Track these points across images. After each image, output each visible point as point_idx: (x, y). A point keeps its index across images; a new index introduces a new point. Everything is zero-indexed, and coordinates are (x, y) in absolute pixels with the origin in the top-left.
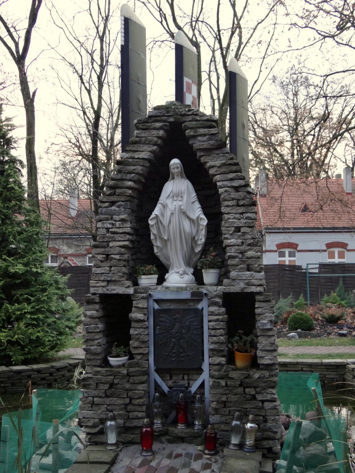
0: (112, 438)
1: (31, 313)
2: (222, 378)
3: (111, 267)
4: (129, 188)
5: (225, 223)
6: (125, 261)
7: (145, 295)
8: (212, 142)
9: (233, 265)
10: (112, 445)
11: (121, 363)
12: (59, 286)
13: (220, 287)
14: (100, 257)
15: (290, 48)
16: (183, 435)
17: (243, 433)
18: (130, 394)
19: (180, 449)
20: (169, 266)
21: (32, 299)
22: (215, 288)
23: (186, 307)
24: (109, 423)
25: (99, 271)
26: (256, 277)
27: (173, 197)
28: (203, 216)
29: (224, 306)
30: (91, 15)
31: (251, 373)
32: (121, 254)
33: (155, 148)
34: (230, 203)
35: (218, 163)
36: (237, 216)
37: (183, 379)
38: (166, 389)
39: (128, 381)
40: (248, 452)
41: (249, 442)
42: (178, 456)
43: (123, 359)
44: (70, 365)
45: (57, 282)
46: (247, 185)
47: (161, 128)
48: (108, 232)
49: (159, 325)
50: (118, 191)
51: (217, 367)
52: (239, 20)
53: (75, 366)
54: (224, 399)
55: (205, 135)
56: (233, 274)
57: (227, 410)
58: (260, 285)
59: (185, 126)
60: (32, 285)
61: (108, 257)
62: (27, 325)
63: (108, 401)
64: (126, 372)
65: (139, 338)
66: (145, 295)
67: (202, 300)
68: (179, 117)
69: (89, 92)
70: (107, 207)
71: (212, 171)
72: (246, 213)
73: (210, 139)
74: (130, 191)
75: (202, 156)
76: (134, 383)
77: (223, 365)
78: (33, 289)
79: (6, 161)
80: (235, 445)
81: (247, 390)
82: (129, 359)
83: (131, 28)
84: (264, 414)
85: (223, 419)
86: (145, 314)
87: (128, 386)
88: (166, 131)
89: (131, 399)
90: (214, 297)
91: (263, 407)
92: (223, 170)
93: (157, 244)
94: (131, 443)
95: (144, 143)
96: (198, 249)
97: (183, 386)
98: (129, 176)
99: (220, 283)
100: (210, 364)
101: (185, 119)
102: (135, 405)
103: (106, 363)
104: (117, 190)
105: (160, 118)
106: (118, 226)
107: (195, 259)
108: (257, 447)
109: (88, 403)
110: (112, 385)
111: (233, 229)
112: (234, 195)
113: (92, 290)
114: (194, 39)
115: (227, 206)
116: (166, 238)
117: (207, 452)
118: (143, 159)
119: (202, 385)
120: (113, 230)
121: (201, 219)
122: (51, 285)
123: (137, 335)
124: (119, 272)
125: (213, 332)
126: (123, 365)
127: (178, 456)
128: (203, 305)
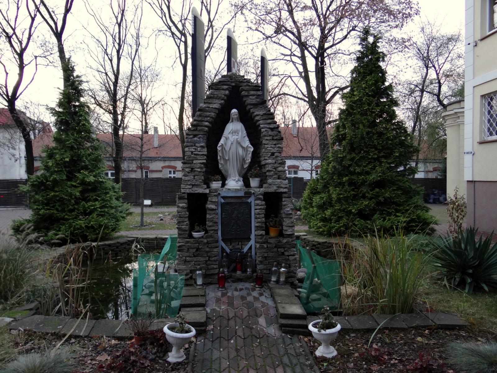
0: (200, 281)
1: (100, 208)
2: (264, 243)
3: (194, 176)
4: (206, 126)
5: (265, 150)
6: (203, 172)
7: (216, 194)
8: (258, 100)
9: (270, 176)
10: (200, 285)
11: (201, 236)
12: (115, 190)
13: (262, 189)
14: (187, 170)
15: (247, 43)
16: (241, 277)
17: (279, 274)
18: (209, 254)
19: (240, 285)
20: (227, 176)
21: (99, 199)
22: (258, 189)
23: (241, 201)
24: (198, 272)
25: (187, 178)
26: (284, 183)
27: (233, 133)
28: (250, 146)
29: (264, 200)
30: (112, 8)
31: (281, 240)
32: (201, 168)
33: (223, 101)
34: (268, 138)
35: (261, 113)
36: (273, 146)
37: (238, 244)
38: (228, 251)
39: (208, 246)
40: (282, 285)
41: (282, 279)
42: (241, 290)
43: (202, 233)
44: (129, 241)
45: (113, 188)
46: (278, 126)
47: (227, 89)
48: (192, 154)
49: (224, 212)
50: (199, 128)
51: (260, 237)
52: (211, 23)
53: (132, 242)
54: (266, 255)
55: (254, 95)
56: (270, 181)
57: (267, 261)
58: (286, 188)
59: (242, 89)
60: (98, 190)
61: (192, 170)
62: (98, 215)
63: (195, 259)
64: (206, 241)
65: (213, 220)
66: (216, 194)
67: (250, 197)
68: (238, 83)
69: (111, 61)
70: (191, 138)
71: (257, 118)
72: (278, 144)
73: (257, 98)
74: (207, 129)
75: (252, 108)
76: (211, 248)
77: (264, 235)
78: (99, 193)
79: (77, 106)
80: (274, 281)
81: (279, 249)
82: (205, 234)
83: (197, 23)
84: (289, 263)
85: (265, 267)
86: (216, 206)
87: (207, 249)
88: (229, 91)
89: (209, 257)
90: (259, 195)
91: (288, 259)
92: (265, 117)
93: (221, 162)
94: (210, 284)
95: (216, 98)
96: (246, 166)
97: (238, 248)
98: (206, 119)
99: (261, 186)
100: (255, 235)
101: (241, 84)
102: (212, 261)
103: (191, 236)
104: (198, 128)
105: (226, 83)
106: (199, 150)
107: (244, 172)
108: (286, 282)
109: (183, 261)
110: (198, 249)
111: (270, 154)
112: (270, 133)
113: (183, 191)
114: (183, 32)
115: (267, 140)
116: (227, 158)
117: (257, 286)
118: (215, 108)
119: (251, 248)
120: (196, 153)
121: (249, 147)
122: (110, 189)
123: (211, 218)
124: (200, 179)
125: (258, 216)
126: (202, 237)
127: (241, 290)
128: (251, 200)
